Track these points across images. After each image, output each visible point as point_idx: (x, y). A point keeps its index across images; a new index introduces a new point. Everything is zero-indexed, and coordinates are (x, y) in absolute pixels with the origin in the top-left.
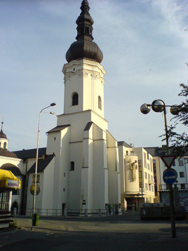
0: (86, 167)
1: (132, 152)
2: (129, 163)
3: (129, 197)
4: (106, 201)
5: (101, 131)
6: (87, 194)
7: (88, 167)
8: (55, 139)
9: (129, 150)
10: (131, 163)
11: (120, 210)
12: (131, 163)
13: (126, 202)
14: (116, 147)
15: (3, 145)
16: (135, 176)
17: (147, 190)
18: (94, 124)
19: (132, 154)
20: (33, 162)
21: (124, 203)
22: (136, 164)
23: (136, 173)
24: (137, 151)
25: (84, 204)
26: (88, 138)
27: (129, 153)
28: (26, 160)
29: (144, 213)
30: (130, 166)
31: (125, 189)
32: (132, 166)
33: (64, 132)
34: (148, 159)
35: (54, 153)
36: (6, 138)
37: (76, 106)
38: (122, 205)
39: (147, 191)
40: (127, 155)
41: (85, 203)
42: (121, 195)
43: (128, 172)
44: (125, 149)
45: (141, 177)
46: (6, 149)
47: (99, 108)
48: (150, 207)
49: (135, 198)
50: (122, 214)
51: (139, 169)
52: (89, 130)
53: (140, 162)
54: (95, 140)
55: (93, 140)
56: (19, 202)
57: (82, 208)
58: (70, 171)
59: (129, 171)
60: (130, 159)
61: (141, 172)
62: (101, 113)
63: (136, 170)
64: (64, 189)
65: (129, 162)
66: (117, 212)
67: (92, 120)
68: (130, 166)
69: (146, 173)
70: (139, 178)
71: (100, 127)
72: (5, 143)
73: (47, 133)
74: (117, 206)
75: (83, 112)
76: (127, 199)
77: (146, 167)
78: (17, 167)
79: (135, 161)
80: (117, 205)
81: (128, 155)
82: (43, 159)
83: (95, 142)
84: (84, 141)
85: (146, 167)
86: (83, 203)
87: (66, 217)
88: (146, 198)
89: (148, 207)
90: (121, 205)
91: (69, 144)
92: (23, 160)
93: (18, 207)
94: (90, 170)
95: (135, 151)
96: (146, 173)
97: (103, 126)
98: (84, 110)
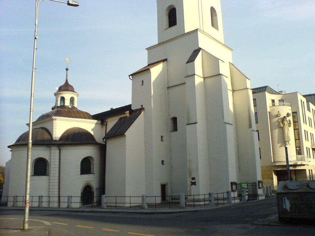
0: (193, 123)
1: (281, 101)
2: (277, 118)
3: (280, 169)
4: (233, 177)
5: (215, 61)
6: (197, 167)
7: (197, 123)
8: (143, 85)
9: (276, 98)
10: (280, 117)
11: (260, 192)
12: (280, 117)
13: (275, 178)
14: (247, 88)
15: (69, 101)
16: (288, 137)
17: (310, 157)
18: (203, 52)
19: (282, 103)
20: (112, 123)
21: (272, 179)
22: (288, 119)
23: (290, 132)
24: (290, 99)
25: (193, 184)
26: (195, 74)
27: (277, 102)
28: (104, 121)
29: (287, 205)
30: (279, 123)
31: (272, 158)
32: (282, 122)
33: (156, 71)
34: (309, 109)
35: (142, 106)
36: (73, 90)
37: (173, 28)
38: (263, 183)
39: (309, 159)
40: (274, 105)
41: (196, 182)
42: (262, 167)
43: (276, 132)
44: (269, 97)
45: (298, 139)
46: (73, 108)
47: (213, 25)
48: (300, 191)
49: (291, 170)
50: (266, 198)
51: (294, 126)
52: (194, 61)
53: (295, 114)
54: (207, 77)
55: (204, 78)
56: (95, 185)
57: (190, 191)
58: (171, 132)
59: (278, 129)
60: (279, 112)
61: (297, 130)
62: (219, 34)
63: (289, 128)
64: (163, 161)
65: (277, 116)
66: (254, 196)
67: (200, 46)
68: (279, 123)
69: (307, 132)
70: (296, 140)
71: (212, 54)
72: (72, 100)
73: (131, 76)
74: (254, 186)
75: (185, 34)
76: (278, 173)
77: (305, 122)
78: (92, 133)
79: (287, 113)
80: (256, 183)
81: (276, 105)
82: (127, 117)
83: (208, 80)
84: (187, 81)
85: (305, 122)
86: (191, 182)
87: (146, 211)
88: (309, 170)
89: (295, 191)
90: (262, 182)
91: (167, 89)
92: (100, 122)
93: (94, 192)
94: (200, 127)
95: (285, 99)
96: (307, 132)
97: (226, 59)
98: (186, 32)
